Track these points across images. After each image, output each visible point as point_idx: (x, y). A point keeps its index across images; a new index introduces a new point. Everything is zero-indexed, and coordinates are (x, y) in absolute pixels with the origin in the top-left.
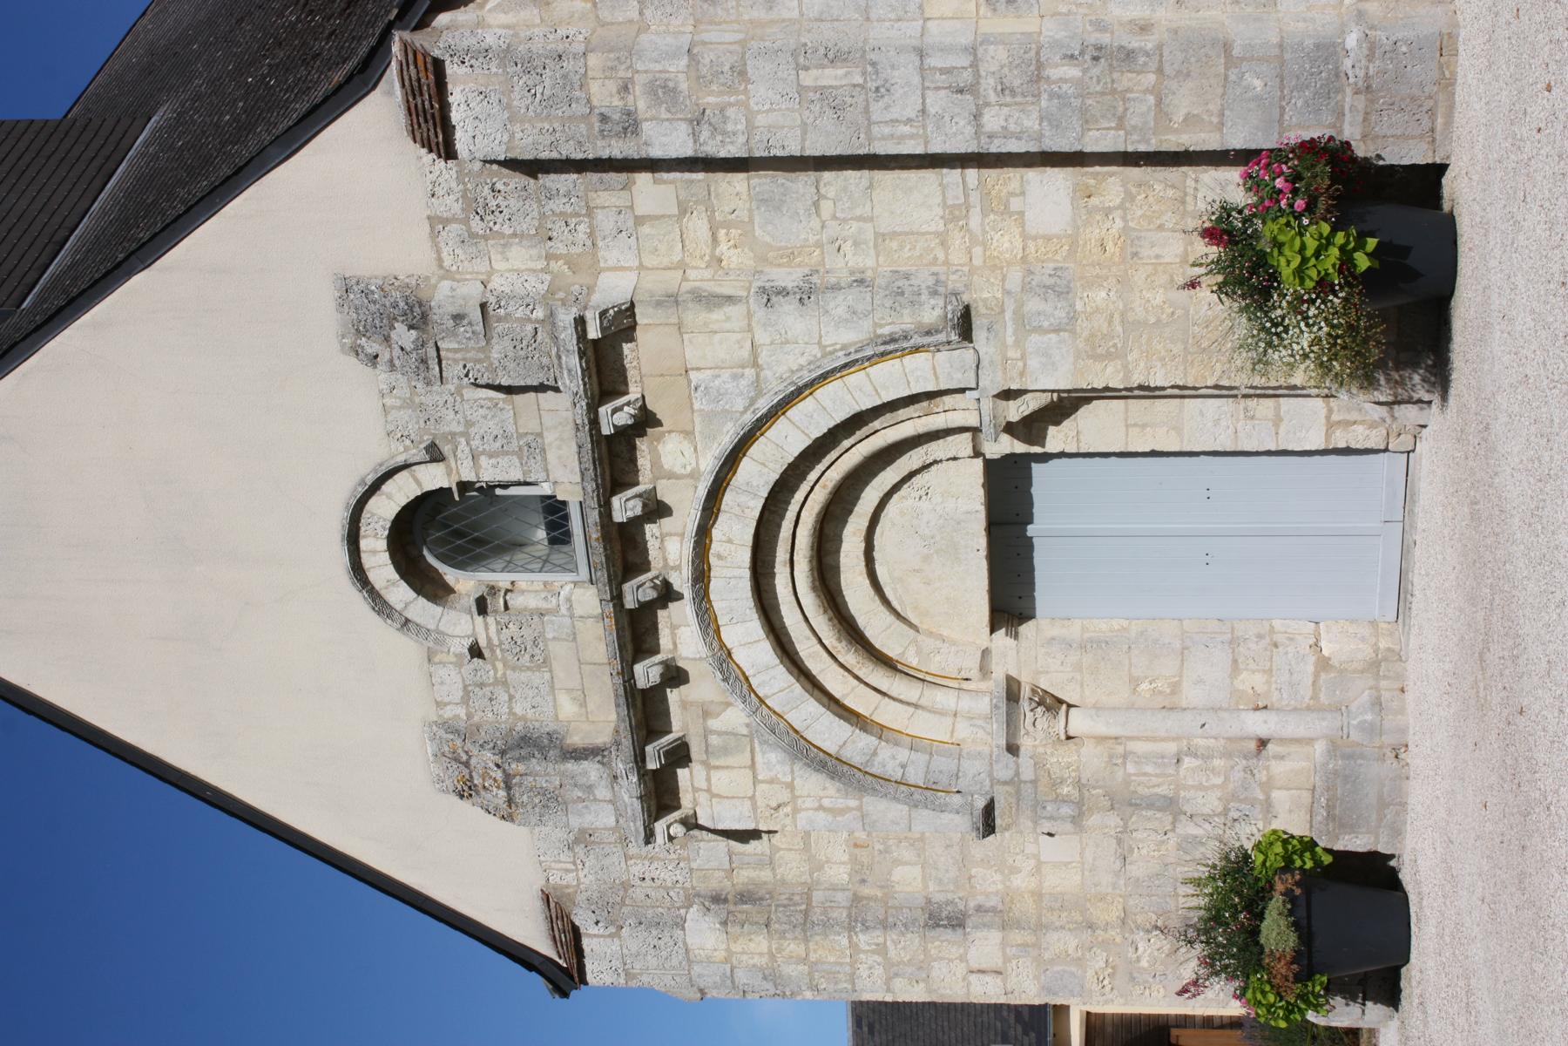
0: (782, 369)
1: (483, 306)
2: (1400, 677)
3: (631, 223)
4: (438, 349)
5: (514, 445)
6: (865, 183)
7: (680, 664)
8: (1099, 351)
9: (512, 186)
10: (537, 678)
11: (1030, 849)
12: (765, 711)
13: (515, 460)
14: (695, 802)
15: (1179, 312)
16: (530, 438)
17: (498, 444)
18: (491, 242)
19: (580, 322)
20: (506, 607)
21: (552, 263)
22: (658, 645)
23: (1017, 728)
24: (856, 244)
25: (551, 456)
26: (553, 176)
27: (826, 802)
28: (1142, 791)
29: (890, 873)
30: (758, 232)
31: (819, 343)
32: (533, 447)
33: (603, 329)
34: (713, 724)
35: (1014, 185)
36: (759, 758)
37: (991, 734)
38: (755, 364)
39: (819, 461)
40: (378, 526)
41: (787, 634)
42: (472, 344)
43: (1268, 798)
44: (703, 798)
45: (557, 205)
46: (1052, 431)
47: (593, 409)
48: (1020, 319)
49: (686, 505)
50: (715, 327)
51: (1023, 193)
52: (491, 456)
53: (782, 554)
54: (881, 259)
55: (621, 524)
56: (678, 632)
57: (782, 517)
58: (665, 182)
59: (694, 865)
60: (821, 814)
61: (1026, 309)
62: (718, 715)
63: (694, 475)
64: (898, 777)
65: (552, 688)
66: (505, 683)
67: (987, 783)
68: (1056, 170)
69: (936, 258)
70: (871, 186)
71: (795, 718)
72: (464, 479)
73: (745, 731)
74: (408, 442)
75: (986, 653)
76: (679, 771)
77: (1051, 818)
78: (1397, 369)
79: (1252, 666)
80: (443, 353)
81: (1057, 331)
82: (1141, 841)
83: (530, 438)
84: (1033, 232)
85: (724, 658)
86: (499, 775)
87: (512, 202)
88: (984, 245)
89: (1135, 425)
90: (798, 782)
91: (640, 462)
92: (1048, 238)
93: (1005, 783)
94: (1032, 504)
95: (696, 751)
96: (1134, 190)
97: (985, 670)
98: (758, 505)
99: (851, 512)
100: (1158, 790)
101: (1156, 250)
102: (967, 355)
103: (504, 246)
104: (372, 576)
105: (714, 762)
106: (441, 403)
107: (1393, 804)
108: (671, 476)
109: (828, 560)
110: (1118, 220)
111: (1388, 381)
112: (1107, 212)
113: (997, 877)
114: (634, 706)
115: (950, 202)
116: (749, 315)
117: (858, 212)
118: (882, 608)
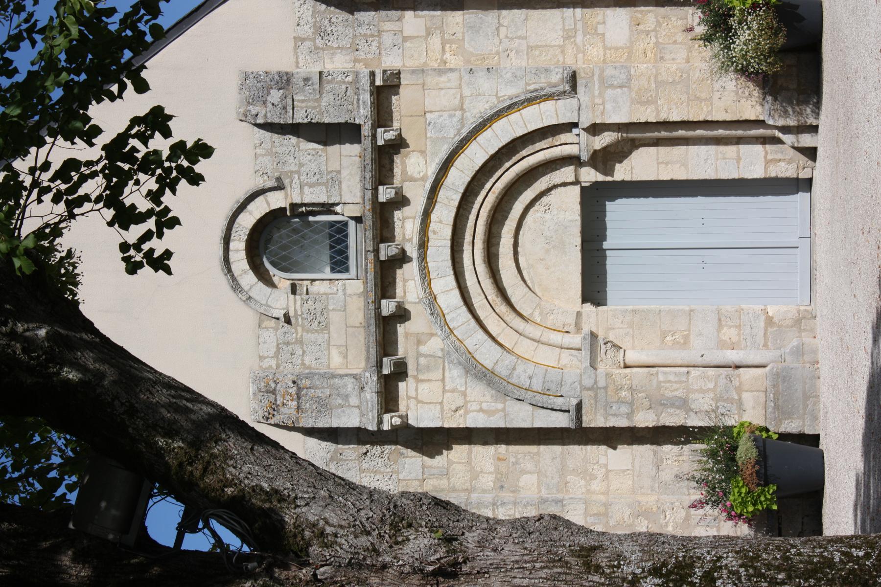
0: (476, 111)
1: (321, 73)
2: (812, 330)
3: (400, 40)
4: (293, 100)
5: (324, 180)
6: (523, 17)
8: (643, 99)
9: (340, 19)
10: (320, 338)
11: (603, 460)
12: (453, 338)
13: (324, 188)
14: (408, 407)
15: (685, 75)
16: (334, 174)
17: (316, 178)
18: (326, 52)
19: (372, 74)
20: (307, 293)
21: (357, 64)
22: (395, 293)
23: (596, 356)
24: (517, 52)
25: (344, 186)
26: (362, 13)
27: (485, 406)
28: (669, 394)
29: (518, 480)
30: (467, 45)
31: (496, 95)
32: (335, 180)
33: (384, 80)
34: (423, 349)
35: (600, 18)
36: (447, 374)
37: (581, 361)
38: (462, 109)
39: (491, 176)
40: (242, 233)
41: (468, 292)
42: (312, 97)
43: (740, 399)
45: (363, 30)
46: (618, 166)
48: (602, 80)
49: (417, 196)
50: (442, 86)
51: (604, 23)
52: (310, 187)
53: (467, 248)
54: (530, 61)
55: (382, 203)
57: (470, 213)
58: (420, 17)
59: (401, 477)
60: (481, 415)
61: (605, 74)
63: (424, 179)
64: (527, 385)
65: (329, 344)
66: (300, 342)
67: (578, 389)
68: (621, 9)
69: (558, 61)
70: (526, 19)
71: (470, 343)
72: (294, 202)
73: (440, 354)
74: (266, 177)
75: (579, 314)
76: (400, 384)
77: (615, 415)
78: (798, 105)
79: (730, 323)
80: (295, 103)
81: (621, 87)
82: (667, 453)
83: (334, 174)
84: (609, 46)
85: (432, 300)
86: (293, 390)
87: (339, 28)
88: (584, 52)
89: (662, 163)
90: (469, 391)
91: (396, 170)
92: (617, 49)
93: (589, 389)
94: (605, 229)
96: (661, 20)
97: (578, 327)
98: (458, 197)
99: (507, 218)
100: (675, 393)
101: (673, 56)
102: (574, 102)
103: (332, 54)
104: (233, 267)
105: (421, 377)
106: (287, 152)
107: (811, 396)
108: (412, 179)
109: (493, 250)
110: (653, 38)
111: (794, 112)
112: (648, 33)
113: (582, 482)
114: (379, 327)
115: (567, 28)
116: (461, 78)
117: (519, 34)
118: (522, 283)
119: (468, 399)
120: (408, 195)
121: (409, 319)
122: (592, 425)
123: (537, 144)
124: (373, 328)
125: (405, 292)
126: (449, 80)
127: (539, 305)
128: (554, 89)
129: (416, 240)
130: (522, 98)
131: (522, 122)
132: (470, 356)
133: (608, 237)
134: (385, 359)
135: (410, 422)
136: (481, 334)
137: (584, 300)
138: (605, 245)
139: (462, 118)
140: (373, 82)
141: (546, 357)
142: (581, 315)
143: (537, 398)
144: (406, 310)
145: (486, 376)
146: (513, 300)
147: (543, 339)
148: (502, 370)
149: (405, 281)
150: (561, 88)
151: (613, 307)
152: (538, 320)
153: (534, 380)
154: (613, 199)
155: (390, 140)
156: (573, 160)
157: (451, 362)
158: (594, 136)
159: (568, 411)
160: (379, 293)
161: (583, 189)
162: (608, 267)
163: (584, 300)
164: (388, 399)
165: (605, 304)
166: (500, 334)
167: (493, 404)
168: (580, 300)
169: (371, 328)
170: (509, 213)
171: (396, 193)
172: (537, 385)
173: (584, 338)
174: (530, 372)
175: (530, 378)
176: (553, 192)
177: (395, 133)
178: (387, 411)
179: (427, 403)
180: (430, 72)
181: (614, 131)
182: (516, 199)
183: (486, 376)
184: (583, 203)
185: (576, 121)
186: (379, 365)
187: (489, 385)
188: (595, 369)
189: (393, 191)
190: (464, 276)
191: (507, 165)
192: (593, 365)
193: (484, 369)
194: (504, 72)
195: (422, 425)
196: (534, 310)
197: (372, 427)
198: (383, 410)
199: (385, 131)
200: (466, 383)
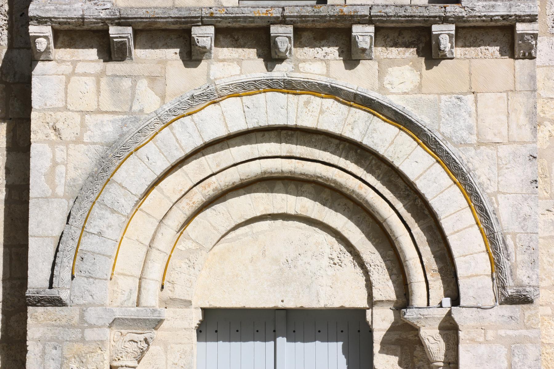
7: (204, 63)
14: (61, 61)
19: (532, 19)
23: (129, 327)
27: (61, 169)
31: (499, 192)
33: (522, 35)
34: (143, 84)
36: (107, 117)
37: (122, 305)
38: (480, 144)
41: (222, 149)
44: (67, 68)
47: (368, 20)
48: (519, 341)
49: (359, 80)
50: (513, 116)
53: (284, 148)
55: (350, 30)
56: (235, 64)
57: (333, 153)
60: (48, 164)
61: (529, 345)
62: (152, 89)
63: (382, 89)
64: (88, 228)
67: (82, 302)
69: (542, 280)
71: (150, 150)
72: (48, 286)
73: (136, 108)
76: (94, 51)
77: (44, 353)
85: (211, 98)
90: (83, 147)
95: (114, 67)
97: (168, 303)
102: (489, 299)
105: (104, 81)
108: (381, 74)
109: (279, 185)
118: (233, 225)
119: (71, 146)
120: (359, 67)
121: (186, 66)
122: (29, 321)
123: (428, 249)
124: (174, 13)
125: (223, 60)
126: (520, 127)
127: (201, 248)
128: (507, 272)
129: (297, 76)
130: (496, 228)
131: (461, 227)
132: (132, 149)
133: (292, 344)
134: (129, 30)
135: (40, 65)
136: (163, 165)
137: (205, 311)
138: (281, 341)
139: (466, 144)
140: (521, 19)
141: (130, 257)
142: (187, 307)
143: (71, 243)
144: (199, 61)
145: (103, 172)
146: (208, 212)
147: (154, 254)
148: (112, 194)
149: (239, 61)
150: (510, 283)
151: (195, 351)
152: (180, 246)
153: (96, 239)
154: (346, 351)
155: (438, 44)
156: (404, 299)
157: (124, 123)
158: (440, 328)
159: (51, 287)
160: (224, 25)
161: (362, 312)
162: (250, 345)
163: (205, 311)
164: (72, 34)
165: (199, 340)
166: (162, 193)
167: (63, 181)
168: (207, 306)
169: (175, 11)
170: (330, 207)
171: (364, 50)
172: (88, 243)
173: (154, 311)
174: (108, 233)
175: (100, 234)
176: (359, 270)
177: (447, 49)
178: (56, 33)
179: (66, 88)
180: (531, 100)
181: (446, 356)
182: (350, 218)
183: (103, 172)
184: (343, 312)
185: (462, 303)
186: (121, 22)
187: (91, 175)
188: (110, 326)
189: (367, 46)
190: (244, 143)
191: (399, 206)
192: (115, 322)
193: (113, 168)
194: (532, 204)
195: (35, 81)
196: (194, 241)
197: (33, 10)
198: (57, 26)
199: (450, 36)
200: (94, 143)
